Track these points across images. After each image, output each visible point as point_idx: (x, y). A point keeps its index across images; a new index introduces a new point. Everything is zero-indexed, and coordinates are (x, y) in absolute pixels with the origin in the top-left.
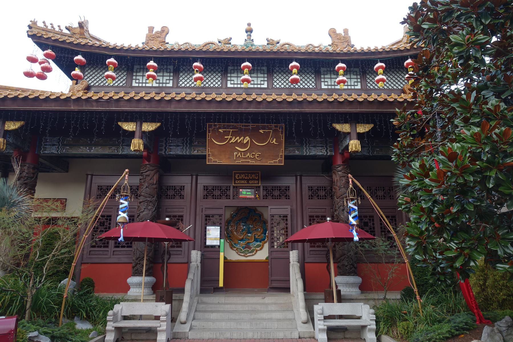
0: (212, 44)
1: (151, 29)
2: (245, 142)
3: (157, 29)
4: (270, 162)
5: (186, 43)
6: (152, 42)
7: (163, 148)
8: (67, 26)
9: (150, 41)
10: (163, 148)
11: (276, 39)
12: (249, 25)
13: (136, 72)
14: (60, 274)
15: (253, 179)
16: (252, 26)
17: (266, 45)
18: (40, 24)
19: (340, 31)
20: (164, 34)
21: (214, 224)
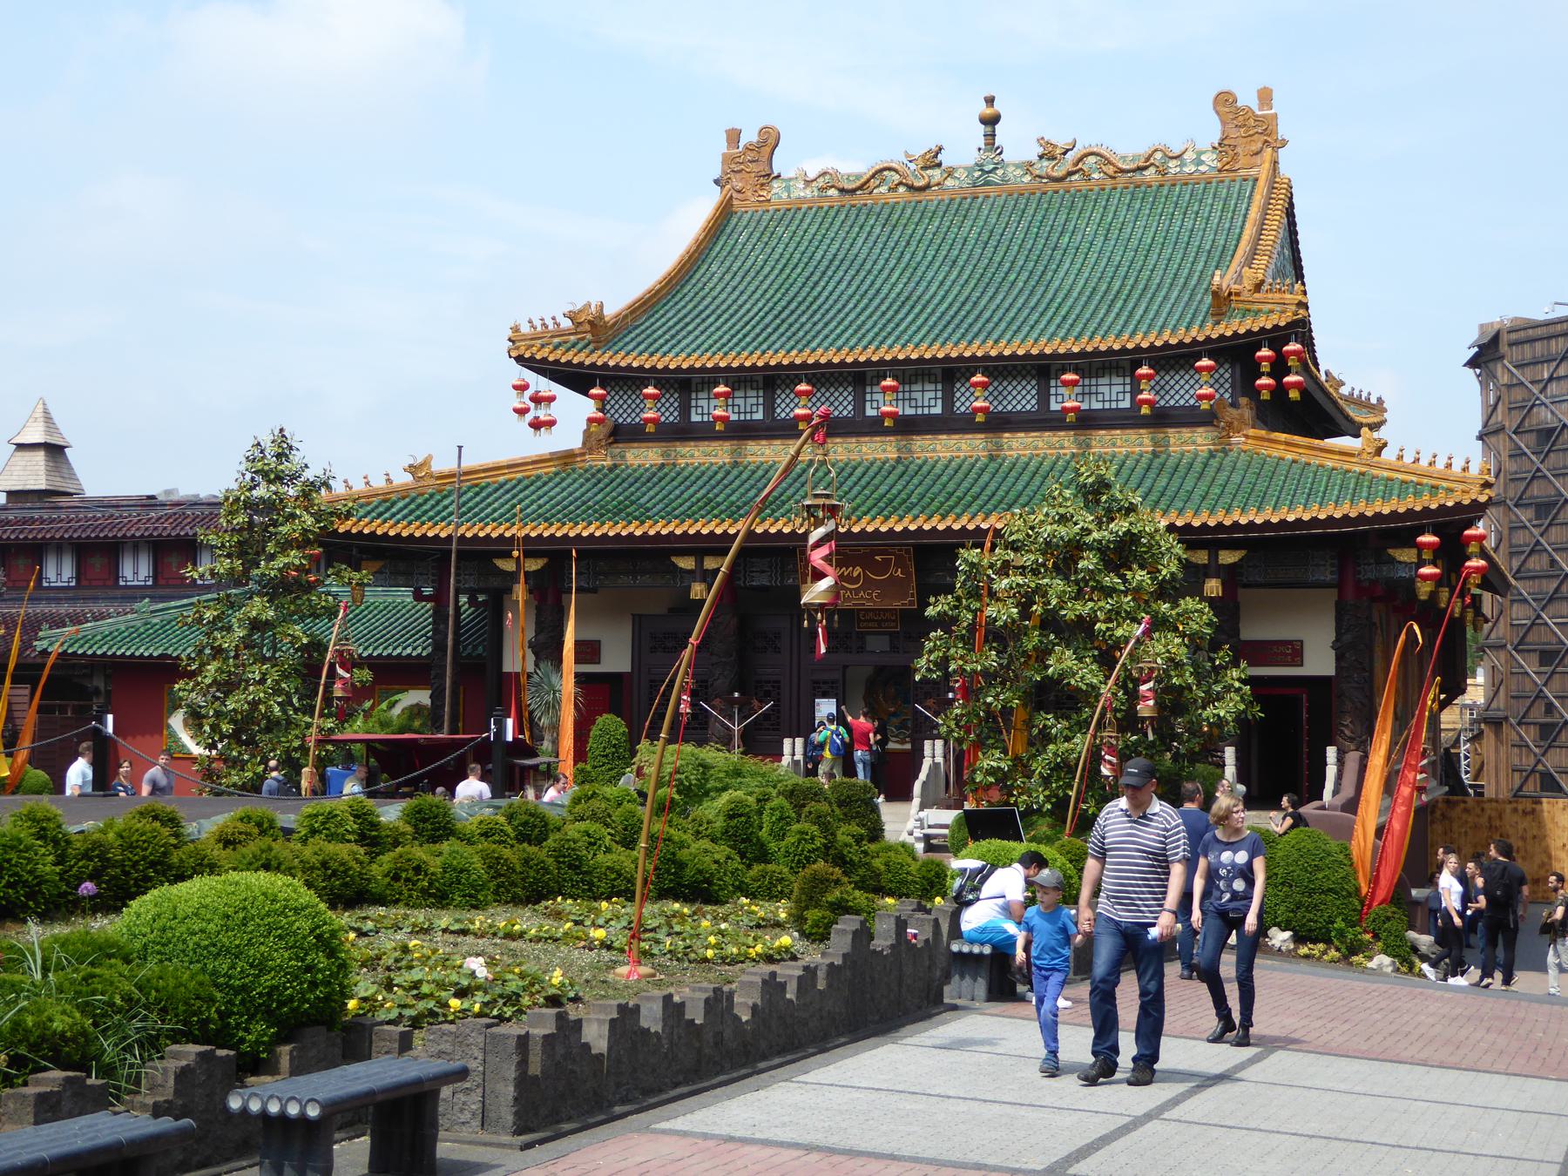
0: (890, 169)
1: (733, 136)
2: (855, 574)
3: (749, 136)
4: (897, 604)
5: (824, 174)
6: (738, 176)
7: (741, 575)
8: (566, 311)
9: (732, 175)
10: (741, 575)
11: (1061, 141)
12: (990, 101)
13: (697, 391)
14: (88, 888)
15: (887, 620)
16: (998, 106)
17: (1035, 158)
18: (525, 329)
19: (1247, 99)
20: (768, 149)
21: (825, 695)
